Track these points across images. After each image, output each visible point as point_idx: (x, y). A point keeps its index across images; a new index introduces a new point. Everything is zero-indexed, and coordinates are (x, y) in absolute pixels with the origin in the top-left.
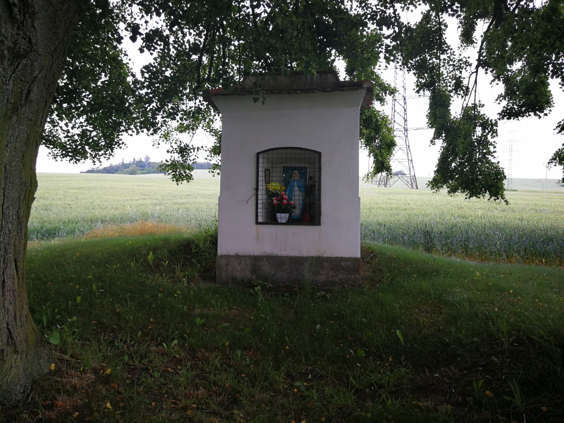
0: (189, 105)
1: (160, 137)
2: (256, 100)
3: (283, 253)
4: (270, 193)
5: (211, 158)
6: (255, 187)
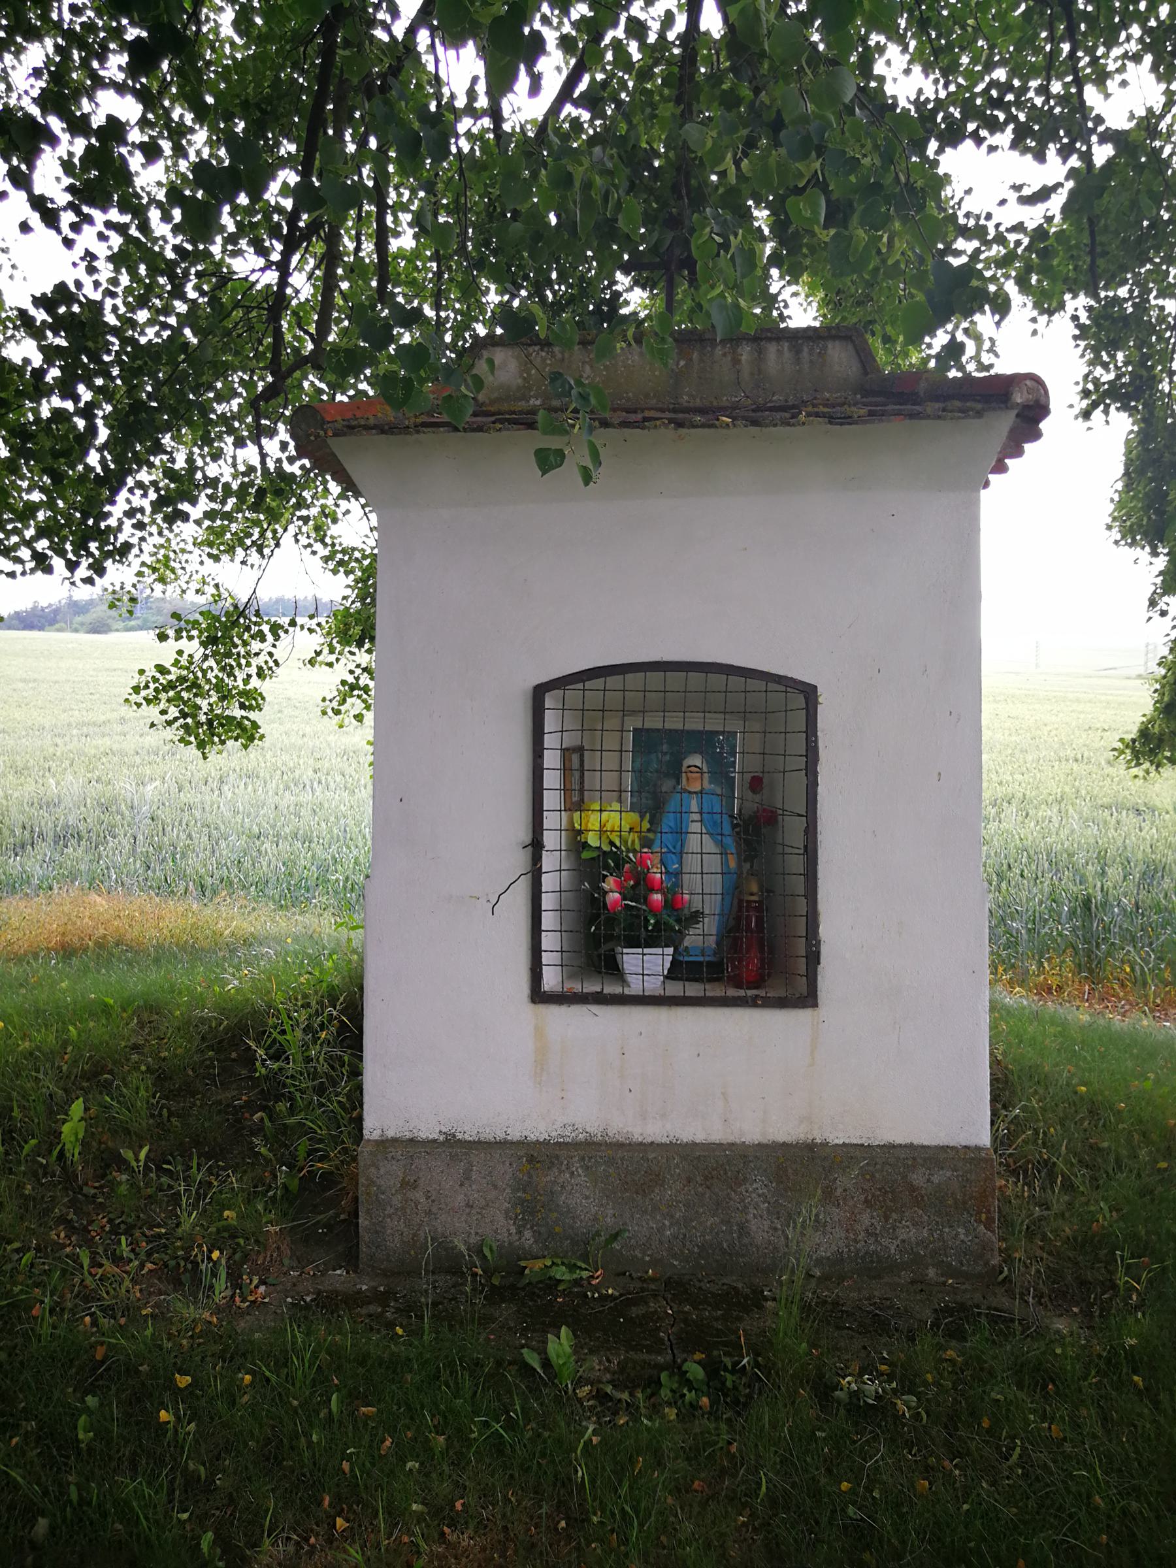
0: (234, 461)
1: (140, 574)
2: (548, 461)
3: (654, 1131)
4: (586, 855)
5: (332, 658)
6: (525, 836)
